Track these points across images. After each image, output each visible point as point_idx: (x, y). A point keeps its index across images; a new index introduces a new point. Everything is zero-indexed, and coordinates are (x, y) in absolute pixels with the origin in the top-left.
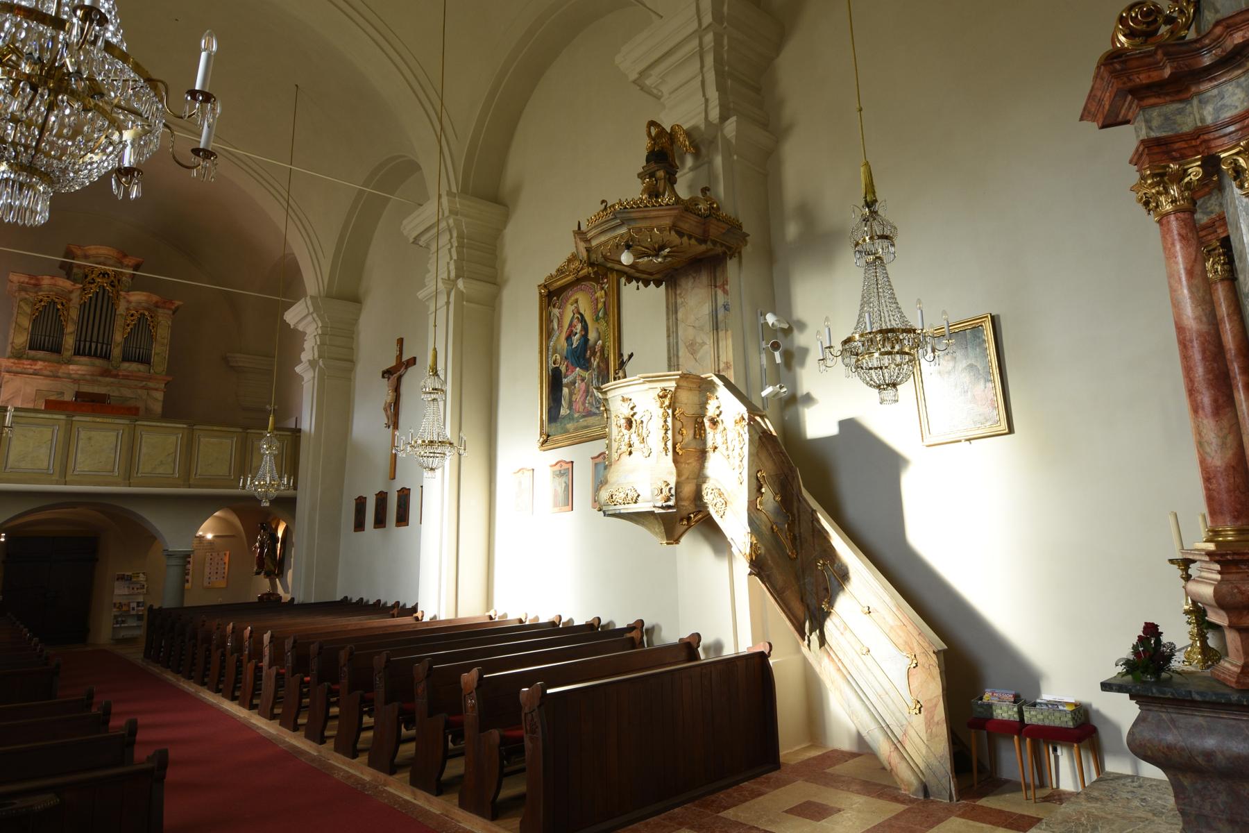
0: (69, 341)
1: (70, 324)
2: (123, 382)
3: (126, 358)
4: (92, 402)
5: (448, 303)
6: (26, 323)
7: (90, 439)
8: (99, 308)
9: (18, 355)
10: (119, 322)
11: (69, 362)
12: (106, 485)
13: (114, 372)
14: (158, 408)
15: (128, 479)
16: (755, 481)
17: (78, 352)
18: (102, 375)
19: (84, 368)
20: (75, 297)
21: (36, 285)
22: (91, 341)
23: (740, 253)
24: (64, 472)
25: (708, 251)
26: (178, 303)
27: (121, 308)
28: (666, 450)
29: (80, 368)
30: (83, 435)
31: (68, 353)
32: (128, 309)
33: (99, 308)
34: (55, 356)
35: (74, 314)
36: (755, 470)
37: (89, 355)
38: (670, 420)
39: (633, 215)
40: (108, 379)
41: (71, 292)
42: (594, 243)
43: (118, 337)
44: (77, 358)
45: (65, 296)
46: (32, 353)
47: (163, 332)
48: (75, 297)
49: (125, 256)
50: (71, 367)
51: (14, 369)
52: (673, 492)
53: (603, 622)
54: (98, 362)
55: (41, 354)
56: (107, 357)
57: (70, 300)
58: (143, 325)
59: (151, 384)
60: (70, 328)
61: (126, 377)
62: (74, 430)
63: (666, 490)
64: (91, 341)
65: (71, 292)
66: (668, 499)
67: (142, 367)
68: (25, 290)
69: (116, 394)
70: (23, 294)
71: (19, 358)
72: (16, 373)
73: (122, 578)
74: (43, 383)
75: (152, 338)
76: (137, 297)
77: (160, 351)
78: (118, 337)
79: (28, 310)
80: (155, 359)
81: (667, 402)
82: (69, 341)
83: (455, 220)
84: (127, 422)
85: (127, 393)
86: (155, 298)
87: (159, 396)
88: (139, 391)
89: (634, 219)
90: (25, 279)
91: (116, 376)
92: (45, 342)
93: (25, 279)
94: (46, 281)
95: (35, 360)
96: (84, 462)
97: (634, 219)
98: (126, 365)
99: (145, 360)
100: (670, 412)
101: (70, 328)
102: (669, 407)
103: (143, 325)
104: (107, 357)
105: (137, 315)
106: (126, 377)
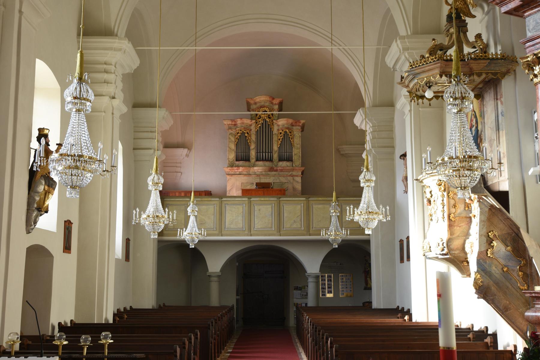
0: (253, 154)
1: (252, 144)
2: (280, 173)
3: (281, 159)
4: (263, 189)
5: (410, 111)
6: (233, 146)
7: (259, 210)
8: (265, 131)
9: (231, 165)
10: (275, 138)
11: (254, 166)
12: (265, 235)
13: (275, 168)
14: (299, 187)
15: (279, 230)
16: (484, 239)
17: (257, 160)
18: (270, 171)
19: (261, 168)
20: (253, 128)
21: (235, 125)
22: (263, 152)
23: (515, 71)
24: (250, 229)
25: (485, 78)
26: (303, 121)
27: (275, 131)
28: (444, 218)
29: (259, 168)
30: (256, 208)
31: (253, 160)
32: (278, 130)
33: (265, 131)
34: (247, 163)
35: (253, 137)
36: (485, 231)
37: (263, 160)
38: (445, 199)
39: (417, 71)
40: (274, 173)
41: (251, 125)
42: (411, 85)
43: (275, 148)
44: (258, 163)
45: (248, 128)
46: (237, 163)
47: (297, 141)
48: (253, 128)
49: (273, 99)
50: (255, 168)
51: (231, 173)
52: (445, 245)
53: (476, 329)
54: (267, 164)
55: (241, 163)
56: (271, 160)
57: (251, 130)
58: (286, 138)
59: (294, 173)
60: (253, 146)
61: (281, 171)
62: (252, 206)
63: (441, 244)
64: (266, 152)
65: (251, 125)
66: (443, 250)
67: (288, 164)
68: (230, 128)
69: (278, 181)
70: (230, 131)
71: (232, 166)
72: (232, 175)
73: (297, 288)
74: (243, 179)
75: (291, 145)
76: (282, 122)
77: (297, 152)
78: (275, 148)
79: (233, 139)
80: (295, 158)
81: (443, 189)
82: (253, 154)
83: (408, 53)
84: (275, 199)
85: (283, 180)
86: (291, 121)
87: (299, 179)
88: (289, 178)
89: (419, 73)
90: (230, 122)
91: (276, 171)
92: (243, 157)
93: (230, 122)
94: (239, 122)
95: (238, 166)
96: (258, 224)
97: (419, 73)
98: (281, 163)
99: (289, 159)
100: (445, 194)
101: (253, 146)
102: (445, 190)
103: (286, 138)
104: (271, 160)
105: (283, 133)
106: (281, 171)
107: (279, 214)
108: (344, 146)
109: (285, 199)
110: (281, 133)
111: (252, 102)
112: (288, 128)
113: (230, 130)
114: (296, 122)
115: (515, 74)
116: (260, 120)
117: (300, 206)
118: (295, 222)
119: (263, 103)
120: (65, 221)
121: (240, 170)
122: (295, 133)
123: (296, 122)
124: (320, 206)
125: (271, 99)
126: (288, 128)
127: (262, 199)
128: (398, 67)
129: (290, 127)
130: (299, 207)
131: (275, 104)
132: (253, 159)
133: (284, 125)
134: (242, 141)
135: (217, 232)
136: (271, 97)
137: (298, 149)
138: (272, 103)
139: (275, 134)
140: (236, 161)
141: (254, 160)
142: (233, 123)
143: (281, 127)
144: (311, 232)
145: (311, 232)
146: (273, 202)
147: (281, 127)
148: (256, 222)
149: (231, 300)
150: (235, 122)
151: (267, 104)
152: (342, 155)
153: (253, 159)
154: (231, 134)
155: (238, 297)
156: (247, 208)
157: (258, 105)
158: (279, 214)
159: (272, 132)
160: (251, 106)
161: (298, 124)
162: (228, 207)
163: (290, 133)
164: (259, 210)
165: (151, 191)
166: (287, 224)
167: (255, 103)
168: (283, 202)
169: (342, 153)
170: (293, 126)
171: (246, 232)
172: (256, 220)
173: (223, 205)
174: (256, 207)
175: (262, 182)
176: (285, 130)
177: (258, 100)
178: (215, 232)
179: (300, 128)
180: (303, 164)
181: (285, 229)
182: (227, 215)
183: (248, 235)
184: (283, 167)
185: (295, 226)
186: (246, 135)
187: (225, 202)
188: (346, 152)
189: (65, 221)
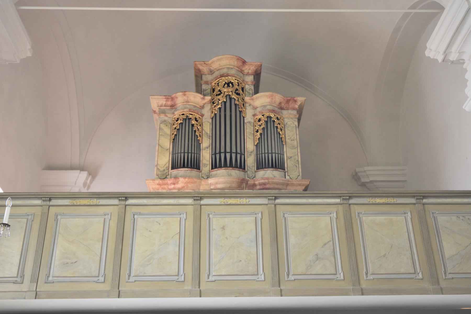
0: (206, 157)
3: (260, 166)
6: (167, 143)
7: (223, 228)
8: (229, 114)
10: (249, 130)
13: (251, 182)
17: (215, 166)
19: (221, 180)
27: (249, 116)
30: (216, 223)
33: (229, 114)
35: (207, 128)
41: (202, 107)
43: (250, 146)
46: (175, 172)
47: (291, 133)
54: (236, 173)
55: (182, 171)
56: (242, 166)
57: (202, 115)
58: (270, 127)
60: (206, 143)
65: (202, 107)
75: (281, 141)
77: (291, 154)
78: (250, 146)
79: (168, 131)
80: (288, 164)
82: (206, 157)
94: (189, 185)
101: (206, 143)
104: (242, 166)
108: (366, 168)
110: (259, 120)
111: (204, 69)
112: (273, 111)
113: (162, 116)
114: (288, 101)
116: (219, 97)
117: (327, 219)
118: (318, 258)
119: (224, 71)
121: (179, 185)
122: (286, 120)
123: (288, 101)
124: (380, 218)
125: (240, 63)
126: (273, 111)
129: (276, 109)
130: (325, 221)
131: (248, 74)
132: (205, 165)
133: (265, 106)
134: (186, 130)
135: (106, 287)
136: (239, 59)
137: (293, 147)
138: (242, 72)
140: (173, 168)
142: (169, 103)
143: (259, 109)
144: (364, 285)
146: (259, 208)
147: (259, 109)
148: (213, 260)
150: (172, 99)
151: (233, 72)
153: (205, 165)
154: (164, 122)
156: (190, 224)
157: (217, 74)
159: (241, 115)
160: (204, 77)
161: (291, 105)
162: (141, 222)
163: (277, 118)
166: (298, 266)
167: (211, 72)
168: (283, 207)
169: (363, 180)
170: (282, 109)
171: (188, 287)
172: (213, 252)
173: (129, 217)
176: (267, 114)
177: (215, 66)
178: (101, 287)
179: (295, 112)
180: (305, 175)
181: (292, 278)
182: (138, 240)
183: (191, 294)
184: (268, 179)
185: (318, 269)
186: (193, 122)
187: (134, 209)
188: (372, 179)
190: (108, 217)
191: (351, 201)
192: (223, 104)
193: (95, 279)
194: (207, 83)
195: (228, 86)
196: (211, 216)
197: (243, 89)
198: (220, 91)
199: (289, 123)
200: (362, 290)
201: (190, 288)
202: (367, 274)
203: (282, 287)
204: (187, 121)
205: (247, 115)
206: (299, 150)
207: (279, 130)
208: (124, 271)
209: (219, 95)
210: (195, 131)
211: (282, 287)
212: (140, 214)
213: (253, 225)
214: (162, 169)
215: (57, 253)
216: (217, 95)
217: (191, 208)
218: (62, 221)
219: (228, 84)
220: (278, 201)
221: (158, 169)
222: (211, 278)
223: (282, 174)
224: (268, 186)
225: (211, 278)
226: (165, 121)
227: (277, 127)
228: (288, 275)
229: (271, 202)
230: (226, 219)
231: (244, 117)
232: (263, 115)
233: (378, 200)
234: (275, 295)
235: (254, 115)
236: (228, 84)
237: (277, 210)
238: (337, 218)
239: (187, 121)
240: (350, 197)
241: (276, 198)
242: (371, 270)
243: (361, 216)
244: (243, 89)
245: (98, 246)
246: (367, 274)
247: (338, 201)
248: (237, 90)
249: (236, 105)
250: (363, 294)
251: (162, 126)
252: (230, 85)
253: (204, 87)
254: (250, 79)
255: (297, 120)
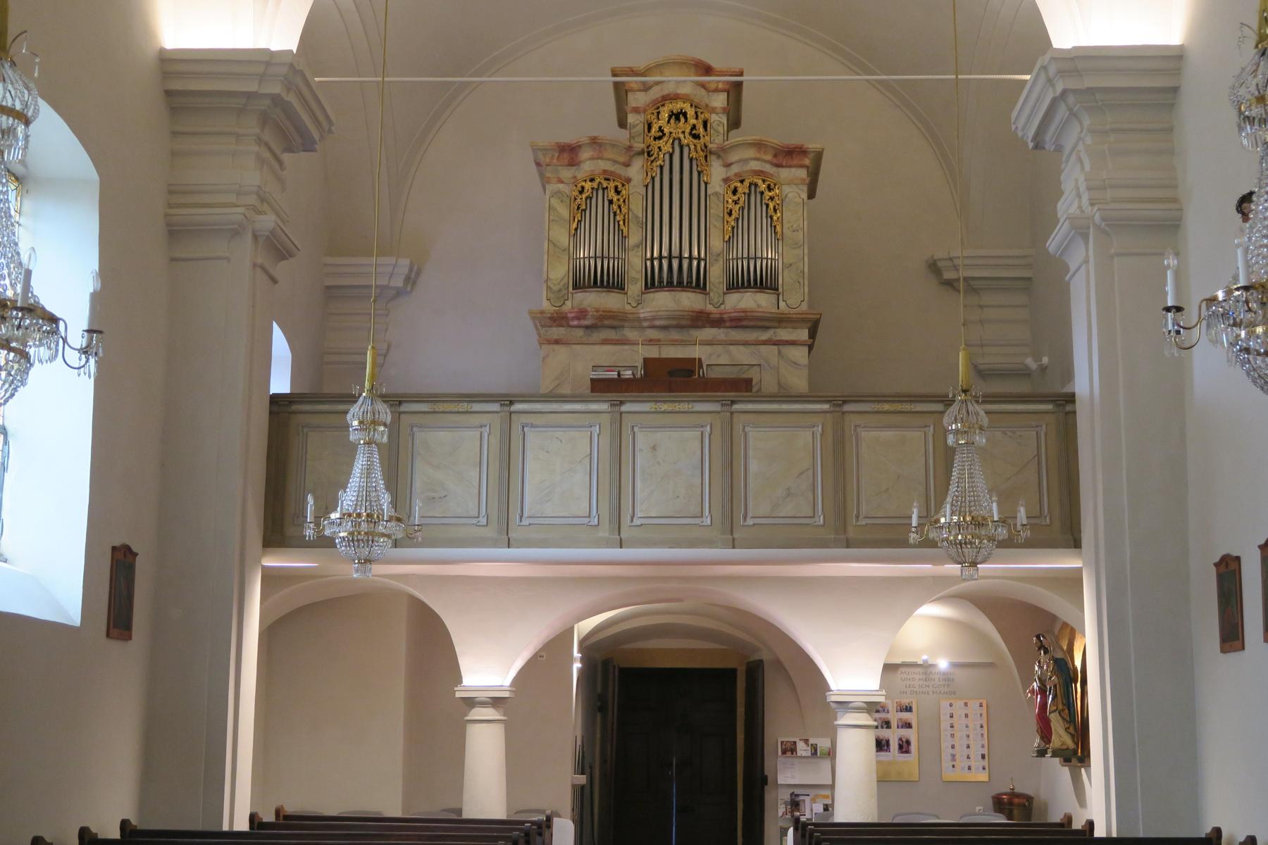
7: (654, 448)
30: (643, 439)
57: (629, 180)
85: (743, 355)
107: (730, 464)
109: (750, 407)
115: (788, 678)
118: (789, 494)
120: (114, 548)
127: (665, 407)
128: (1049, 137)
130: (804, 438)
132: (635, 281)
139: (716, 194)
141: (640, 285)
144: (851, 533)
145: (851, 533)
146: (707, 419)
148: (639, 497)
149: (556, 793)
152: (950, 284)
153: (635, 281)
155: (582, 779)
158: (730, 464)
160: (630, 96)
162: (531, 435)
164: (654, 448)
165: (352, 449)
168: (743, 417)
171: (604, 533)
172: (639, 484)
174: (641, 437)
175: (664, 356)
181: (750, 522)
183: (608, 544)
185: (788, 509)
187: (524, 419)
189: (114, 548)
190: (486, 431)
191: (847, 408)
192: (667, 157)
193: (474, 521)
194: (636, 110)
195: (678, 119)
196: (636, 429)
197: (705, 124)
198: (661, 129)
199: (790, 195)
200: (847, 540)
201: (607, 534)
202: (857, 517)
203: (736, 536)
204: (600, 192)
205: (713, 179)
206: (806, 251)
207: (771, 212)
208: (514, 516)
209: (660, 138)
210: (615, 214)
211: (736, 536)
212: (532, 426)
213: (698, 444)
214: (556, 288)
215: (418, 484)
216: (655, 139)
217: (606, 419)
218: (420, 435)
219: (677, 116)
220: (736, 407)
221: (548, 288)
222: (637, 522)
223: (773, 298)
224: (745, 323)
225: (637, 522)
226: (559, 192)
227: (767, 206)
228: (745, 519)
229: (725, 408)
230: (659, 434)
231: (706, 184)
232: (742, 182)
233: (886, 407)
234: (725, 546)
235: (726, 180)
236: (677, 116)
237: (735, 420)
238: (822, 435)
239: (600, 192)
240: (845, 402)
241: (733, 402)
242: (864, 510)
243: (859, 430)
244: (705, 124)
245: (475, 474)
246: (857, 517)
247: (826, 407)
248: (694, 127)
249: (691, 160)
250: (848, 547)
251: (554, 202)
252: (682, 119)
253: (632, 118)
254: (720, 101)
255: (805, 188)
